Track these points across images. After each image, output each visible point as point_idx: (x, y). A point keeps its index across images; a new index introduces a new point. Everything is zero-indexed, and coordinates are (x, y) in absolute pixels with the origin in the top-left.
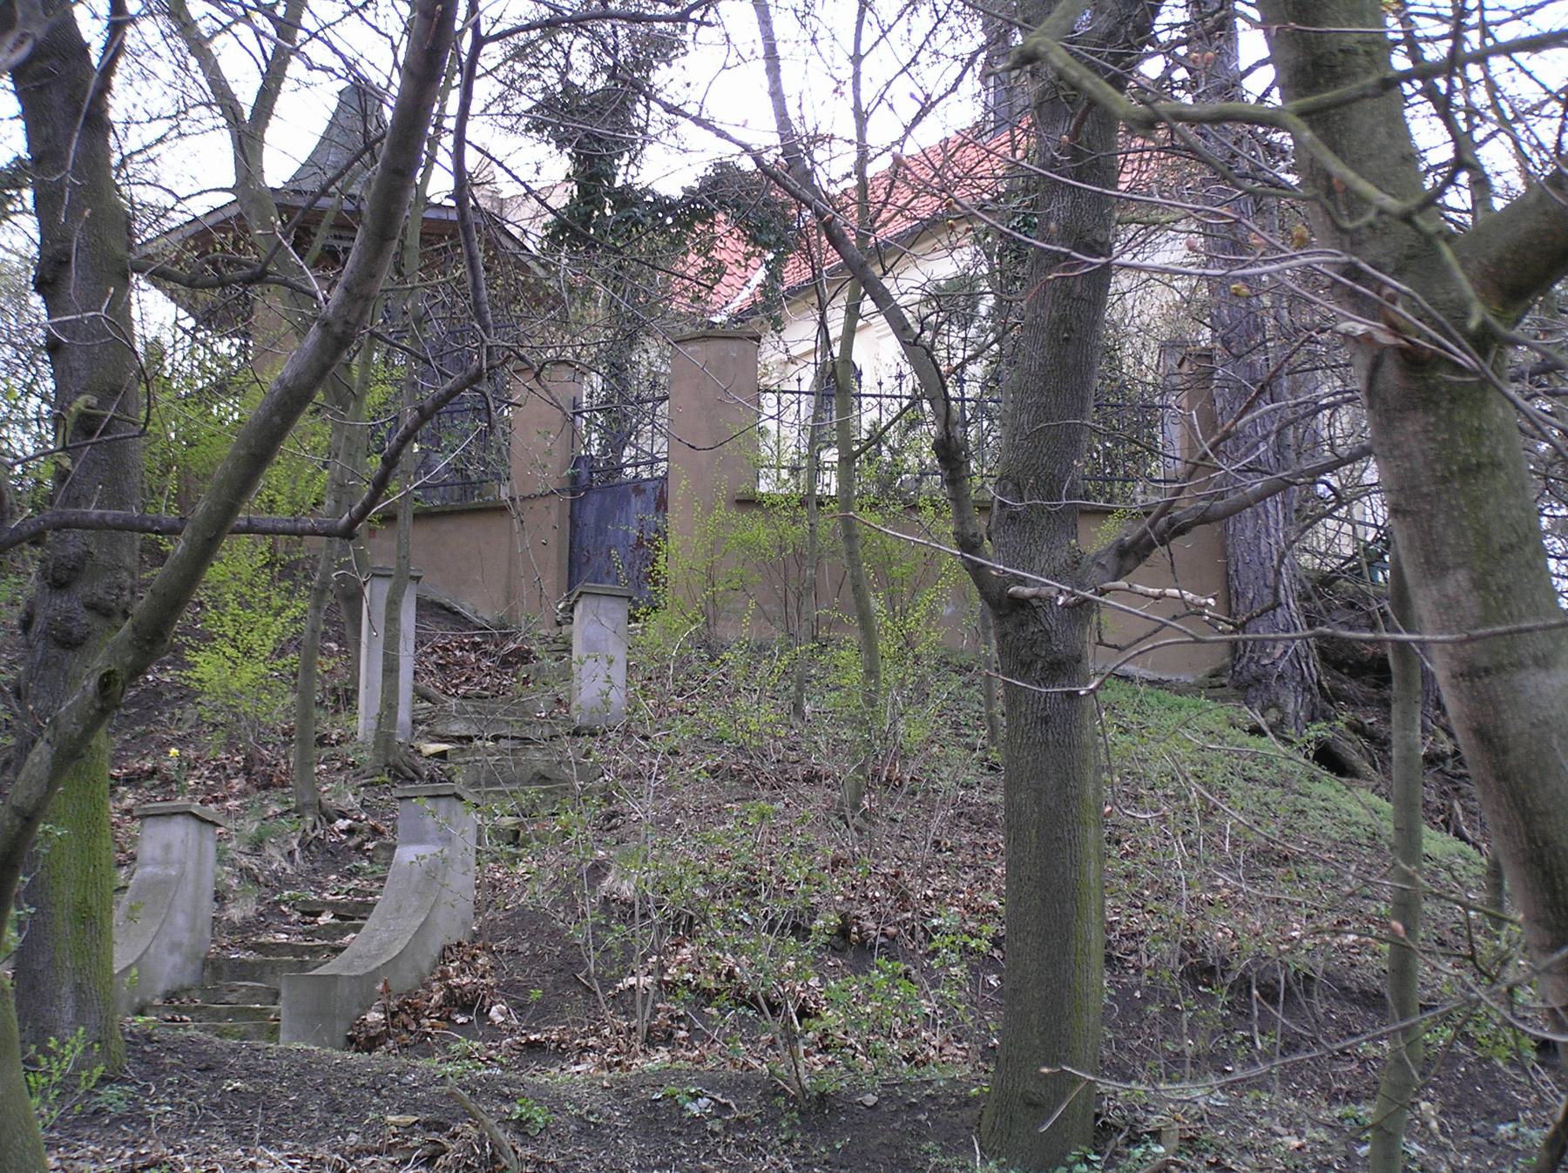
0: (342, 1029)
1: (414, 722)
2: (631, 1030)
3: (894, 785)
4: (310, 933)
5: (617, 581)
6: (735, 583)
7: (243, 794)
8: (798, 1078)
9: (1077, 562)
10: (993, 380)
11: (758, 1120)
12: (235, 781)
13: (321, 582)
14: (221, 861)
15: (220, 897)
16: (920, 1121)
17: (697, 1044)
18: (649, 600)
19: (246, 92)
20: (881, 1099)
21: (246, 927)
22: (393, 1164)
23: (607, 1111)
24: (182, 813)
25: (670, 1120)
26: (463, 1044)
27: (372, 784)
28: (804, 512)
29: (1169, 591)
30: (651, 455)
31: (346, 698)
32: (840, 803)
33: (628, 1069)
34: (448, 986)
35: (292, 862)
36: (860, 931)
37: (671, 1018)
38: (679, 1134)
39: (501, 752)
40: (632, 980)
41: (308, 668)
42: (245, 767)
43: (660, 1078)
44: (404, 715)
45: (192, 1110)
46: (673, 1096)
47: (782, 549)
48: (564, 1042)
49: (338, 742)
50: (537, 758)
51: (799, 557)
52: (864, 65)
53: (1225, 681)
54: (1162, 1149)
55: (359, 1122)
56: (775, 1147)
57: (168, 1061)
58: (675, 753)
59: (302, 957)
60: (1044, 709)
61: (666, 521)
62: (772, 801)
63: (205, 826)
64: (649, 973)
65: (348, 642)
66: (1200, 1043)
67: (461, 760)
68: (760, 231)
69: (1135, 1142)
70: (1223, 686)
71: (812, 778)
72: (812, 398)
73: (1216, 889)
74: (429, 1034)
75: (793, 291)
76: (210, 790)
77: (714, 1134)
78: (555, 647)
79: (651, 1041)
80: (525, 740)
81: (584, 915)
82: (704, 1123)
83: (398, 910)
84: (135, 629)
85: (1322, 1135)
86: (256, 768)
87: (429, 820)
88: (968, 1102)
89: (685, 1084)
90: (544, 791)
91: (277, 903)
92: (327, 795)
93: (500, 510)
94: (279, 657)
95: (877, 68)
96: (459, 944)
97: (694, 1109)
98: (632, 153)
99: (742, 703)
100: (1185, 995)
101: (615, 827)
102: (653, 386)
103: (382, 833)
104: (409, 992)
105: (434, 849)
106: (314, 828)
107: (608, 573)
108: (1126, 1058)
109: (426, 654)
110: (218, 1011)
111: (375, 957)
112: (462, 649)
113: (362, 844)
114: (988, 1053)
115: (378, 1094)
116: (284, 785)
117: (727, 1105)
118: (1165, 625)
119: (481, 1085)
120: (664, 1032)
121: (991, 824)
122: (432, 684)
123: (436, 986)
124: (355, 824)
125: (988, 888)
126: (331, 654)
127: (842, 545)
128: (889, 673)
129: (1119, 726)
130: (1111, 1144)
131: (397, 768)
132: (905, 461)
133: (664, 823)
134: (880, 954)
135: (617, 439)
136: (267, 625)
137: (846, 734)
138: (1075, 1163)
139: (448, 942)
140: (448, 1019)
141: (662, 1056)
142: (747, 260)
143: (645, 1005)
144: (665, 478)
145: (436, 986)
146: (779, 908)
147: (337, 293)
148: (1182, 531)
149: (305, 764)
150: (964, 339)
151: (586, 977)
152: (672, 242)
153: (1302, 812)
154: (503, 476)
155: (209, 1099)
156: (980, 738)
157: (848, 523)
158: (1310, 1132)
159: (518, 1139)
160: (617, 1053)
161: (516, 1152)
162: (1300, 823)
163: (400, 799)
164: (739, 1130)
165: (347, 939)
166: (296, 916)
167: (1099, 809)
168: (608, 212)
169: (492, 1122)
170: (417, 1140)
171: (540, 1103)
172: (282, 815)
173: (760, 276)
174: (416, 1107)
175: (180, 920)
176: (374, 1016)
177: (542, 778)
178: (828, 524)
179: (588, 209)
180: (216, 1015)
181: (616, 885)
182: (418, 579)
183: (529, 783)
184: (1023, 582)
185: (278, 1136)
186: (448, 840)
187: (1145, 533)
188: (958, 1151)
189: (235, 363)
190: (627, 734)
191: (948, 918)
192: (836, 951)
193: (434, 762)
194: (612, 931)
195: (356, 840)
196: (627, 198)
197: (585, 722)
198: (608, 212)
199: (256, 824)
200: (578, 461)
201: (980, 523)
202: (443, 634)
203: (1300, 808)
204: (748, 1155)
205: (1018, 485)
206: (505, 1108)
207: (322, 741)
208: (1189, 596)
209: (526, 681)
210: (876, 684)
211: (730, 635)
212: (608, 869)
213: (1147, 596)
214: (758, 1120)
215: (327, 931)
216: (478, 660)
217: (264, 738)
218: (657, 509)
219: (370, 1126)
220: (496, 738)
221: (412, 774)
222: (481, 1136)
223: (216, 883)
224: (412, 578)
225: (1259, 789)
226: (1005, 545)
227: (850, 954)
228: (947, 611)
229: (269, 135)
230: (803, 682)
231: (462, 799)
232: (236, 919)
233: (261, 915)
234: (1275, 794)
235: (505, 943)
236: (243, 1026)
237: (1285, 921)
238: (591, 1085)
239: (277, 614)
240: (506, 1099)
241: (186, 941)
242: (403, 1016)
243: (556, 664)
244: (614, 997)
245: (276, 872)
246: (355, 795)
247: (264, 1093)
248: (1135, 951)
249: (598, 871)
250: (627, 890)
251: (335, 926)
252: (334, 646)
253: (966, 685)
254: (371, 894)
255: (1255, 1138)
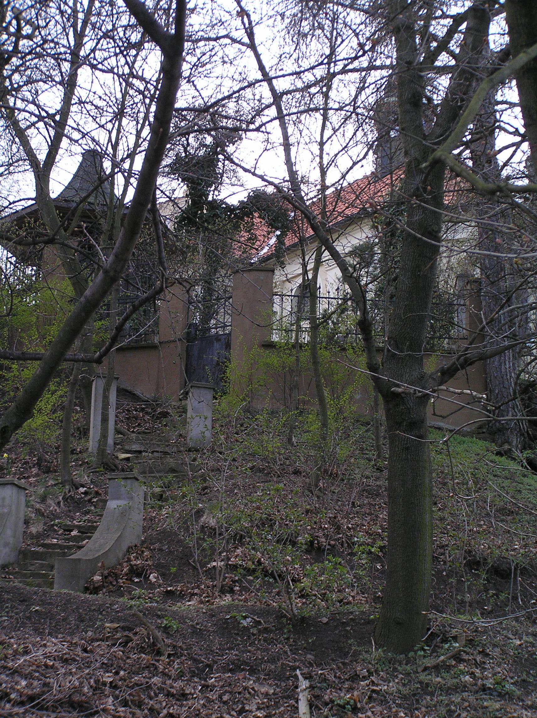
0: (82, 583)
1: (115, 444)
2: (214, 586)
3: (333, 476)
4: (68, 539)
5: (207, 381)
6: (262, 383)
7: (37, 475)
8: (292, 610)
9: (423, 377)
10: (380, 291)
11: (274, 628)
12: (33, 469)
13: (74, 380)
14: (27, 506)
15: (27, 522)
16: (347, 630)
17: (244, 593)
18: (223, 390)
19: (42, 157)
20: (330, 620)
21: (38, 536)
22: (108, 645)
23: (205, 623)
24: (11, 484)
25: (234, 628)
26: (137, 591)
27: (96, 472)
28: (294, 351)
29: (465, 391)
30: (224, 323)
31: (84, 432)
32: (310, 484)
33: (213, 604)
34: (131, 565)
35: (59, 507)
36: (318, 543)
37: (232, 581)
38: (238, 634)
39: (154, 458)
40: (214, 564)
41: (68, 418)
42: (37, 463)
43: (229, 609)
44: (110, 441)
45: (17, 619)
46: (235, 617)
47: (284, 368)
48: (183, 591)
49: (80, 452)
50: (171, 461)
51: (291, 371)
52: (325, 147)
53: (484, 430)
54: (457, 645)
55: (92, 626)
56: (281, 641)
57: (6, 596)
58: (234, 460)
59: (64, 551)
60: (407, 444)
61: (230, 354)
62: (279, 482)
63: (20, 490)
64: (222, 561)
65: (85, 405)
66: (473, 596)
67: (136, 461)
68: (274, 221)
69: (445, 641)
70: (483, 433)
71: (297, 472)
72: (297, 298)
73: (480, 526)
74: (122, 587)
75: (288, 249)
76: (22, 473)
77: (254, 635)
78: (178, 410)
79: (223, 591)
80: (166, 453)
81: (193, 534)
82: (249, 629)
83: (108, 529)
84: (17, 407)
85: (531, 639)
86: (43, 464)
87: (123, 489)
88: (369, 622)
89: (241, 611)
90: (174, 477)
91: (53, 525)
92: (76, 477)
93: (154, 347)
94: (53, 413)
95: (331, 148)
96: (136, 546)
97: (245, 623)
98: (217, 185)
99: (265, 438)
100: (466, 574)
101: (207, 493)
102: (225, 291)
103: (100, 494)
104: (113, 567)
105: (125, 502)
106: (69, 491)
107: (203, 377)
108: (439, 602)
109: (119, 413)
110: (26, 574)
111: (99, 551)
112: (136, 411)
113: (91, 499)
114: (377, 599)
115: (101, 613)
116: (56, 471)
117: (259, 622)
118: (464, 406)
119: (148, 610)
120: (229, 587)
121: (378, 495)
122: (123, 427)
123: (125, 564)
124: (88, 490)
125: (376, 524)
126: (77, 412)
127: (311, 366)
128: (332, 425)
129: (436, 451)
130: (434, 642)
131: (107, 464)
132: (339, 327)
133: (230, 492)
134: (328, 554)
135: (207, 317)
136: (48, 398)
137: (312, 453)
138: (418, 650)
139: (130, 545)
140: (131, 580)
141: (228, 599)
142: (268, 234)
143: (220, 575)
144: (230, 334)
145: (125, 564)
146: (284, 533)
147: (111, 258)
148: (471, 364)
149: (66, 462)
150: (367, 272)
151: (194, 562)
152: (234, 226)
153: (519, 491)
154: (156, 332)
155: (24, 614)
156: (372, 454)
157: (314, 355)
158: (525, 638)
159: (165, 635)
160: (207, 597)
161: (164, 641)
162: (519, 496)
163: (110, 479)
164: (265, 633)
165: (85, 542)
166: (60, 532)
167: (431, 490)
168: (205, 212)
169: (154, 627)
170: (119, 635)
171: (175, 619)
172: (55, 485)
173: (273, 241)
174: (118, 620)
175: (9, 532)
176: (97, 578)
177: (173, 471)
178: (305, 356)
179: (196, 210)
180: (25, 576)
181: (207, 520)
182: (117, 378)
183: (167, 473)
184: (398, 386)
185: (56, 632)
186: (131, 498)
187: (454, 363)
188: (365, 644)
189: (34, 278)
190: (213, 451)
191: (360, 537)
192: (307, 551)
193: (124, 462)
194: (206, 541)
195: (89, 497)
196: (215, 205)
197: (193, 445)
198: (205, 212)
199: (43, 489)
200: (190, 326)
201: (379, 359)
202: (127, 404)
203: (518, 489)
204: (269, 644)
205: (396, 341)
206: (159, 621)
207: (73, 452)
208: (474, 393)
209: (166, 425)
210: (326, 430)
211: (259, 407)
212: (204, 513)
213: (455, 393)
214: (274, 628)
215: (75, 538)
216: (143, 416)
217: (46, 450)
218: (226, 348)
219: (97, 628)
220: (153, 452)
221: (114, 468)
222: (148, 634)
223: (25, 516)
224: (115, 378)
225: (500, 480)
226: (390, 369)
227: (314, 553)
228: (358, 397)
229: (53, 175)
230: (292, 428)
231: (138, 480)
232: (34, 532)
233: (45, 530)
234: (507, 483)
235: (157, 545)
236: (38, 581)
237: (512, 541)
238: (198, 611)
239: (52, 394)
240: (159, 617)
241: (11, 542)
242: (110, 578)
243: (179, 419)
244: (206, 571)
245: (52, 511)
246: (88, 476)
247: (49, 612)
248: (443, 554)
249: (199, 513)
250: (212, 522)
251: (79, 536)
252: (79, 409)
253: (367, 431)
254: (96, 522)
255: (500, 640)
